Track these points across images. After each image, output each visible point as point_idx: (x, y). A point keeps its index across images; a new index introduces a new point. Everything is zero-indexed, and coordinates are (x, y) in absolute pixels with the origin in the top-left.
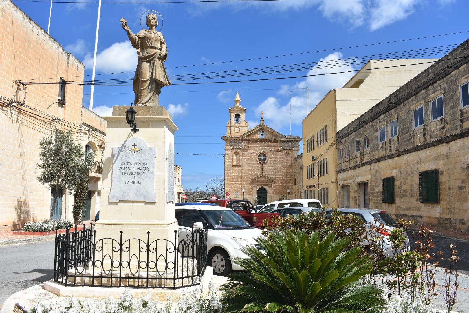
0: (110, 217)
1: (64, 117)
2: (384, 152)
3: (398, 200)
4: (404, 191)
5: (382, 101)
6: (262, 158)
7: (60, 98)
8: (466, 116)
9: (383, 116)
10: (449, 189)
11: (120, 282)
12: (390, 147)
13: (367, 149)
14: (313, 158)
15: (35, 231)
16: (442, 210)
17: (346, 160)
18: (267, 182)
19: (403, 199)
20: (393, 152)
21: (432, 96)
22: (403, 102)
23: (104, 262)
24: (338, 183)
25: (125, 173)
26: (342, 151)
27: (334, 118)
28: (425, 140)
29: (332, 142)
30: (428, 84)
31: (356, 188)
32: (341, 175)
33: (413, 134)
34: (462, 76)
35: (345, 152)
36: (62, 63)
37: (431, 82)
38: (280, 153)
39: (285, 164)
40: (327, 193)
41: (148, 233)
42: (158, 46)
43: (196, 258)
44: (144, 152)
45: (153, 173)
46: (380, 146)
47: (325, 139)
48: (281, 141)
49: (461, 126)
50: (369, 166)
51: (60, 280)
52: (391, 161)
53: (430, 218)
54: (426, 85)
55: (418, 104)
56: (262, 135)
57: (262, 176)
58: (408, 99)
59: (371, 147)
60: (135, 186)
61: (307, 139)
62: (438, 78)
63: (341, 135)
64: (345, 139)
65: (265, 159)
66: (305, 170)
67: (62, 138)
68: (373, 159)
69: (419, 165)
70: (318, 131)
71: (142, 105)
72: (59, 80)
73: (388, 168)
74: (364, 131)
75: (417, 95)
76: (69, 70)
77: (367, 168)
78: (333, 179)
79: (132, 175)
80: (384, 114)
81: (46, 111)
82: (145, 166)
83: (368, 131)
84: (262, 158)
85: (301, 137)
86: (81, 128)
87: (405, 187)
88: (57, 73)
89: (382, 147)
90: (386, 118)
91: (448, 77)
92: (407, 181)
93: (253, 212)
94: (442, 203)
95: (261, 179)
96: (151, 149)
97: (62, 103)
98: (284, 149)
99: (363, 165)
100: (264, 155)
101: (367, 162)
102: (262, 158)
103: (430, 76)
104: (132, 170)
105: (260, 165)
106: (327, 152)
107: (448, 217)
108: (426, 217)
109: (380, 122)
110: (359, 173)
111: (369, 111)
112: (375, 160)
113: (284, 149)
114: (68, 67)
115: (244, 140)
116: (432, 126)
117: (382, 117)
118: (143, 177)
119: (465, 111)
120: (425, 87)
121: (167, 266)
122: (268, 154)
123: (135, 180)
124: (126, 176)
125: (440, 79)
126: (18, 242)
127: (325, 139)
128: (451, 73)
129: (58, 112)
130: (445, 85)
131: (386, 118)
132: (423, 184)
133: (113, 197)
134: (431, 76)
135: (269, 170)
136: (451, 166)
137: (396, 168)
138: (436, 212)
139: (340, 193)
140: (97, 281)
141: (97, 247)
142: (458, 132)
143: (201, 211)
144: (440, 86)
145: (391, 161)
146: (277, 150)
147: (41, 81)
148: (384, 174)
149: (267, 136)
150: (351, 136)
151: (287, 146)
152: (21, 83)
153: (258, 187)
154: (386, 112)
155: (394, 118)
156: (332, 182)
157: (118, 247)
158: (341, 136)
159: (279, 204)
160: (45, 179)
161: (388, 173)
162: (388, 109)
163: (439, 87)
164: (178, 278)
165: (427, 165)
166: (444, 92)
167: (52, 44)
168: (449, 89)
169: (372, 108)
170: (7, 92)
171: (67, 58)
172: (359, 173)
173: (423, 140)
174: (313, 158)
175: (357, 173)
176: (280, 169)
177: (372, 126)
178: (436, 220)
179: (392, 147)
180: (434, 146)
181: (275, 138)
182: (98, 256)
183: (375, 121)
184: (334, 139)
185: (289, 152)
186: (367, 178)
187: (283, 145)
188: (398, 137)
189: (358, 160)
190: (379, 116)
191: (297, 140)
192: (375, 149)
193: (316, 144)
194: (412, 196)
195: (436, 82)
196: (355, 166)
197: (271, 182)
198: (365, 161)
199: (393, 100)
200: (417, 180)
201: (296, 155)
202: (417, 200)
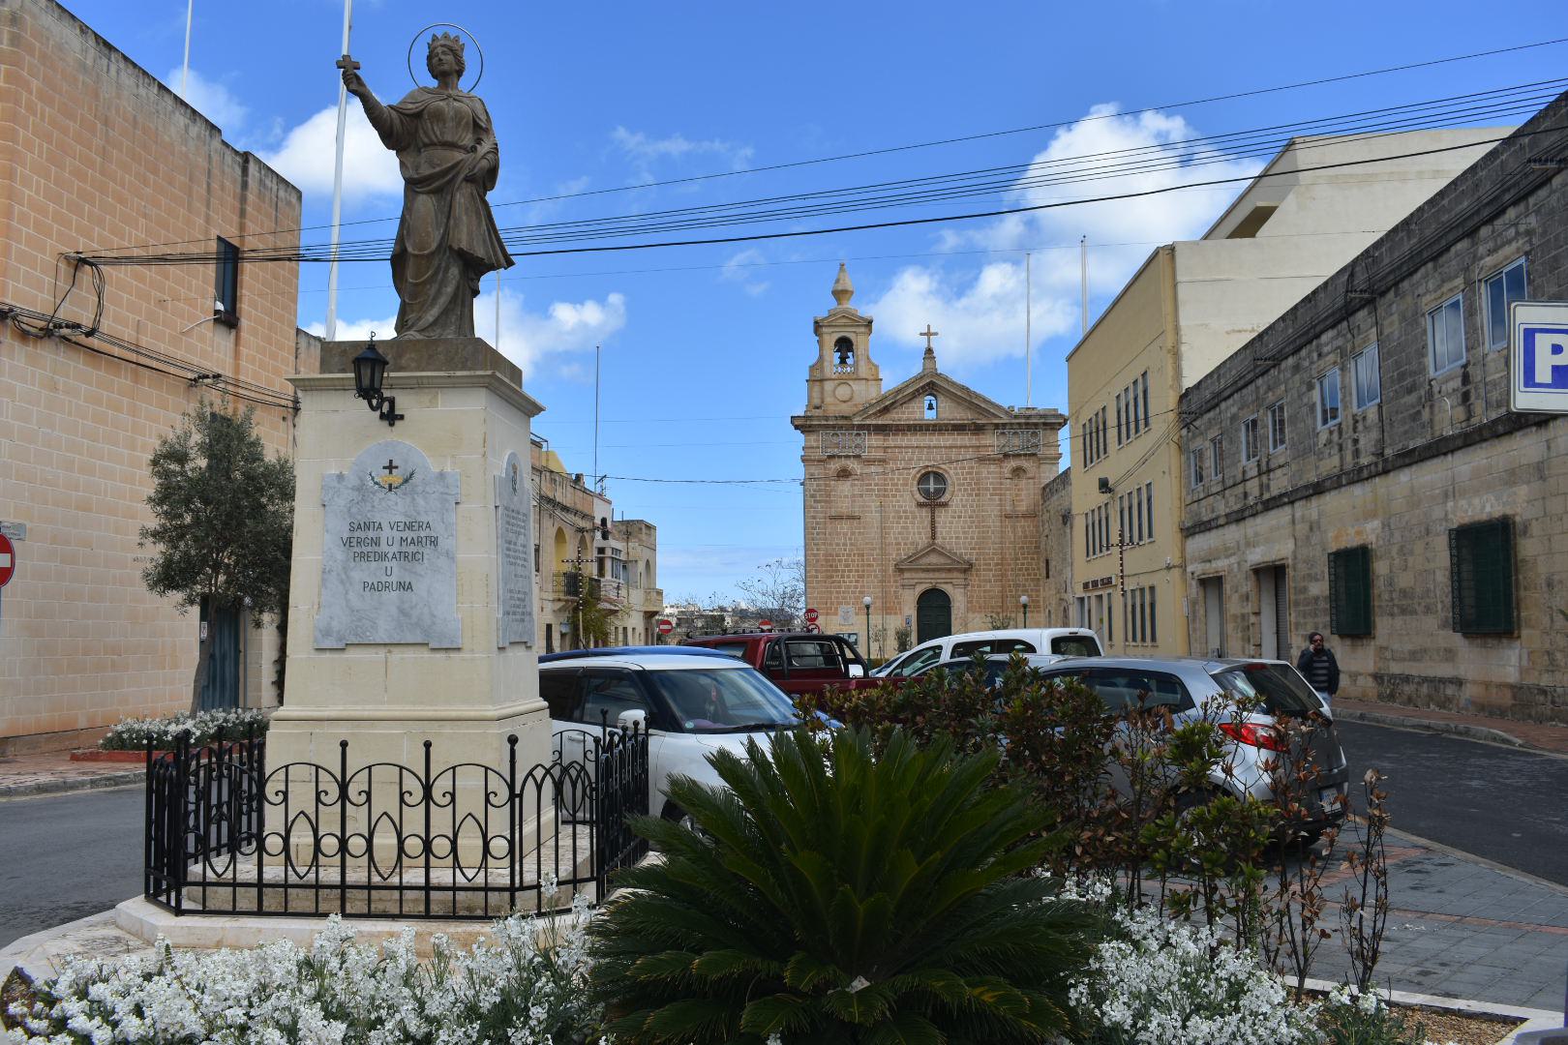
0: (329, 702)
1: (237, 369)
2: (1336, 461)
3: (1383, 625)
4: (1404, 593)
5: (1326, 283)
6: (932, 490)
7: (220, 306)
9: (1330, 334)
10: (1550, 585)
11: (346, 900)
12: (1356, 441)
13: (1281, 448)
14: (1104, 486)
16: (1525, 657)
17: (1214, 490)
18: (950, 570)
19: (1399, 621)
20: (1364, 461)
21: (1489, 261)
22: (1396, 284)
23: (293, 840)
24: (1189, 569)
25: (363, 556)
26: (1199, 455)
27: (1169, 345)
28: (1469, 416)
29: (1164, 427)
30: (1476, 219)
31: (1248, 586)
32: (1200, 543)
33: (1430, 394)
35: (1209, 463)
36: (222, 187)
37: (1485, 213)
38: (992, 468)
40: (1152, 606)
41: (428, 745)
42: (468, 139)
43: (590, 823)
44: (420, 489)
45: (450, 556)
46: (1323, 438)
47: (1141, 415)
48: (997, 426)
50: (1287, 509)
51: (163, 899)
52: (1359, 492)
53: (1487, 685)
54: (1470, 224)
55: (1445, 289)
56: (930, 407)
57: (932, 549)
58: (1411, 274)
60: (392, 597)
61: (1084, 420)
62: (1507, 197)
63: (1195, 401)
64: (1207, 416)
65: (940, 492)
67: (226, 438)
68: (1301, 483)
69: (1450, 504)
70: (1119, 389)
71: (419, 336)
72: (213, 246)
73: (1347, 518)
74: (1269, 389)
75: (1442, 260)
76: (249, 209)
77: (1280, 517)
78: (1172, 558)
79: (386, 563)
80: (1333, 326)
81: (172, 351)
82: (423, 534)
83: (1284, 384)
84: (932, 486)
85: (1066, 413)
87: (1404, 581)
88: (208, 219)
89: (1329, 442)
90: (1340, 342)
91: (1542, 193)
92: (1411, 560)
93: (856, 671)
94: (1525, 632)
95: (934, 559)
96: (442, 475)
97: (228, 320)
98: (1006, 456)
99: (1270, 505)
100: (939, 477)
101: (1281, 496)
102: (932, 486)
103: (1481, 192)
104: (384, 548)
105: (925, 513)
106: (1151, 461)
107: (1545, 681)
108: (1475, 682)
109: (1320, 355)
110: (1256, 534)
111: (1282, 318)
112: (1306, 487)
113: (1006, 456)
114: (243, 200)
115: (867, 427)
116: (1491, 366)
117: (1324, 338)
118: (418, 567)
120: (1469, 229)
121: (486, 851)
122: (952, 473)
123: (394, 579)
124: (364, 564)
125: (1515, 203)
126: (82, 784)
127: (1141, 415)
128: (1549, 180)
129: (213, 351)
130: (1533, 221)
131: (1340, 342)
132: (1465, 567)
134: (1487, 190)
135: (955, 529)
136: (1556, 505)
137: (1374, 515)
138: (1509, 664)
139: (1194, 603)
140: (266, 901)
141: (270, 790)
143: (643, 675)
144: (1516, 225)
145: (1357, 490)
146: (981, 460)
147: (152, 252)
148: (1337, 537)
150: (1229, 408)
151: (1016, 442)
152: (84, 261)
153: (920, 589)
154: (1340, 322)
155: (1366, 340)
156: (1169, 568)
157: (419, 793)
158: (1198, 406)
159: (957, 646)
160: (168, 577)
161: (1351, 531)
162: (1347, 312)
163: (1512, 231)
164: (522, 888)
165: (1476, 501)
166: (1527, 248)
167: (187, 127)
168: (1544, 233)
169: (1295, 308)
170: (32, 292)
171: (238, 171)
172: (1256, 534)
173: (1463, 417)
174: (1104, 486)
175: (1250, 532)
176: (993, 522)
177: (1297, 368)
178: (1508, 694)
179: (1362, 444)
180: (1498, 436)
181: (977, 417)
182: (274, 819)
183: (1303, 352)
184: (1172, 416)
186: (1281, 549)
187: (1003, 441)
188: (1380, 406)
189: (1253, 487)
190: (1318, 336)
191: (1051, 423)
192: (1305, 450)
193: (1112, 433)
194: (1428, 610)
195: (1502, 211)
196: (1242, 511)
197: (965, 571)
198: (1275, 492)
199: (1361, 278)
200: (1441, 556)
201: (1048, 475)
202: (1444, 626)
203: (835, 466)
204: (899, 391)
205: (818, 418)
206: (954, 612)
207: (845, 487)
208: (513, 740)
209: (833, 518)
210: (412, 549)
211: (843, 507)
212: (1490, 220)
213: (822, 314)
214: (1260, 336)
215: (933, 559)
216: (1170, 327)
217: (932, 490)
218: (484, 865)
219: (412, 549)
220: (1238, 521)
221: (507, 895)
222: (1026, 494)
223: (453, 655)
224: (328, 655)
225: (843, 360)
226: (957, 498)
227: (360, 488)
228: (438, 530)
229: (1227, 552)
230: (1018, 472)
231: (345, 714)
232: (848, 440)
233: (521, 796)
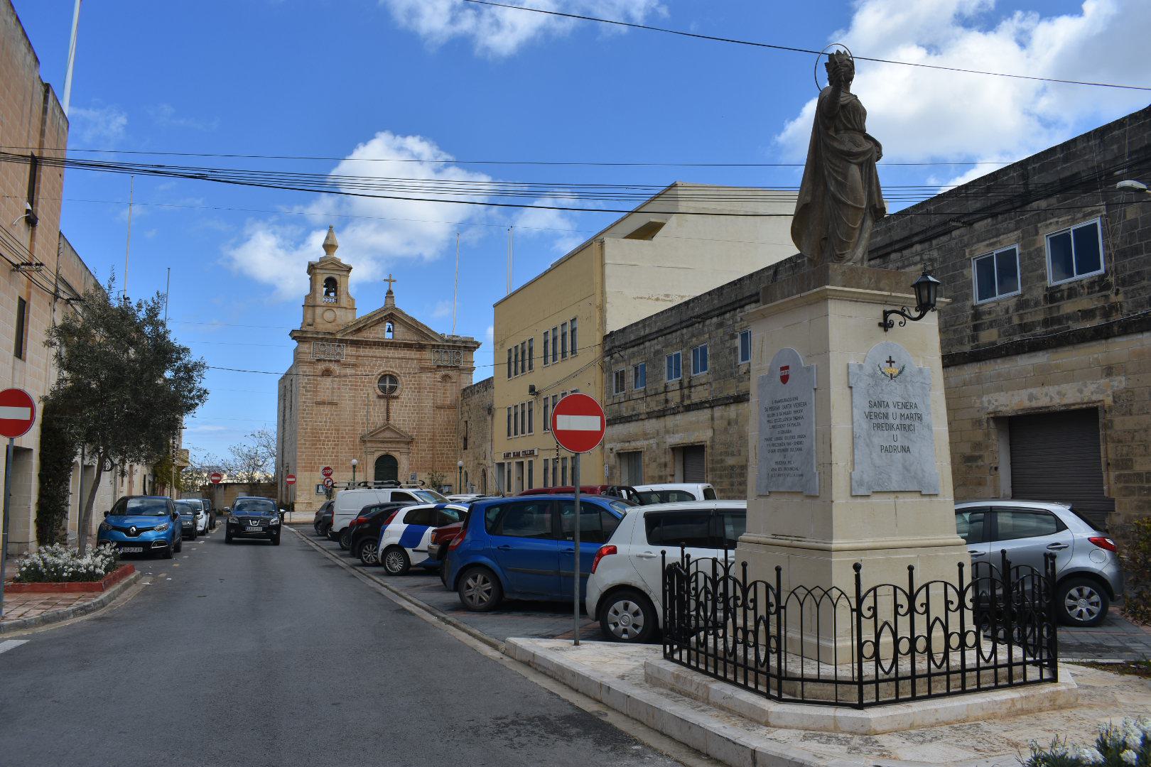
6: (388, 386)
8: (987, 318)
14: (532, 389)
15: (59, 578)
25: (879, 426)
26: (621, 377)
27: (598, 302)
34: (979, 241)
37: (897, 247)
39: (439, 402)
45: (929, 427)
48: (434, 346)
49: (974, 338)
56: (389, 330)
57: (387, 427)
59: (714, 371)
60: (898, 456)
65: (393, 389)
66: (501, 418)
74: (693, 336)
77: (705, 414)
86: (57, 290)
91: (944, 239)
95: (388, 434)
96: (809, 369)
99: (689, 408)
100: (393, 379)
104: (891, 421)
105: (383, 402)
111: (709, 293)
112: (727, 398)
115: (345, 341)
119: (985, 308)
122: (402, 380)
125: (921, 242)
128: (950, 232)
130: (935, 254)
133: (861, 484)
135: (403, 414)
139: (611, 468)
142: (967, 348)
144: (921, 255)
146: (423, 369)
149: (402, 334)
151: (446, 359)
153: (377, 455)
158: (615, 344)
163: (918, 258)
169: (722, 287)
174: (532, 389)
177: (720, 325)
181: (421, 339)
183: (728, 315)
185: (450, 373)
186: (702, 435)
187: (437, 356)
195: (911, 246)
203: (321, 367)
204: (369, 318)
205: (313, 333)
206: (400, 471)
207: (327, 382)
208: (857, 567)
209: (318, 403)
210: (907, 422)
211: (324, 395)
212: (900, 250)
213: (315, 259)
214: (687, 303)
215: (388, 434)
216: (598, 292)
217: (388, 386)
218: (895, 661)
219: (907, 422)
220: (658, 417)
221: (893, 684)
222: (450, 394)
223: (934, 499)
224: (859, 500)
225: (327, 293)
226: (405, 393)
227: (873, 376)
228: (921, 409)
229: (646, 436)
230: (446, 378)
231: (878, 545)
232: (331, 348)
233: (785, 608)
